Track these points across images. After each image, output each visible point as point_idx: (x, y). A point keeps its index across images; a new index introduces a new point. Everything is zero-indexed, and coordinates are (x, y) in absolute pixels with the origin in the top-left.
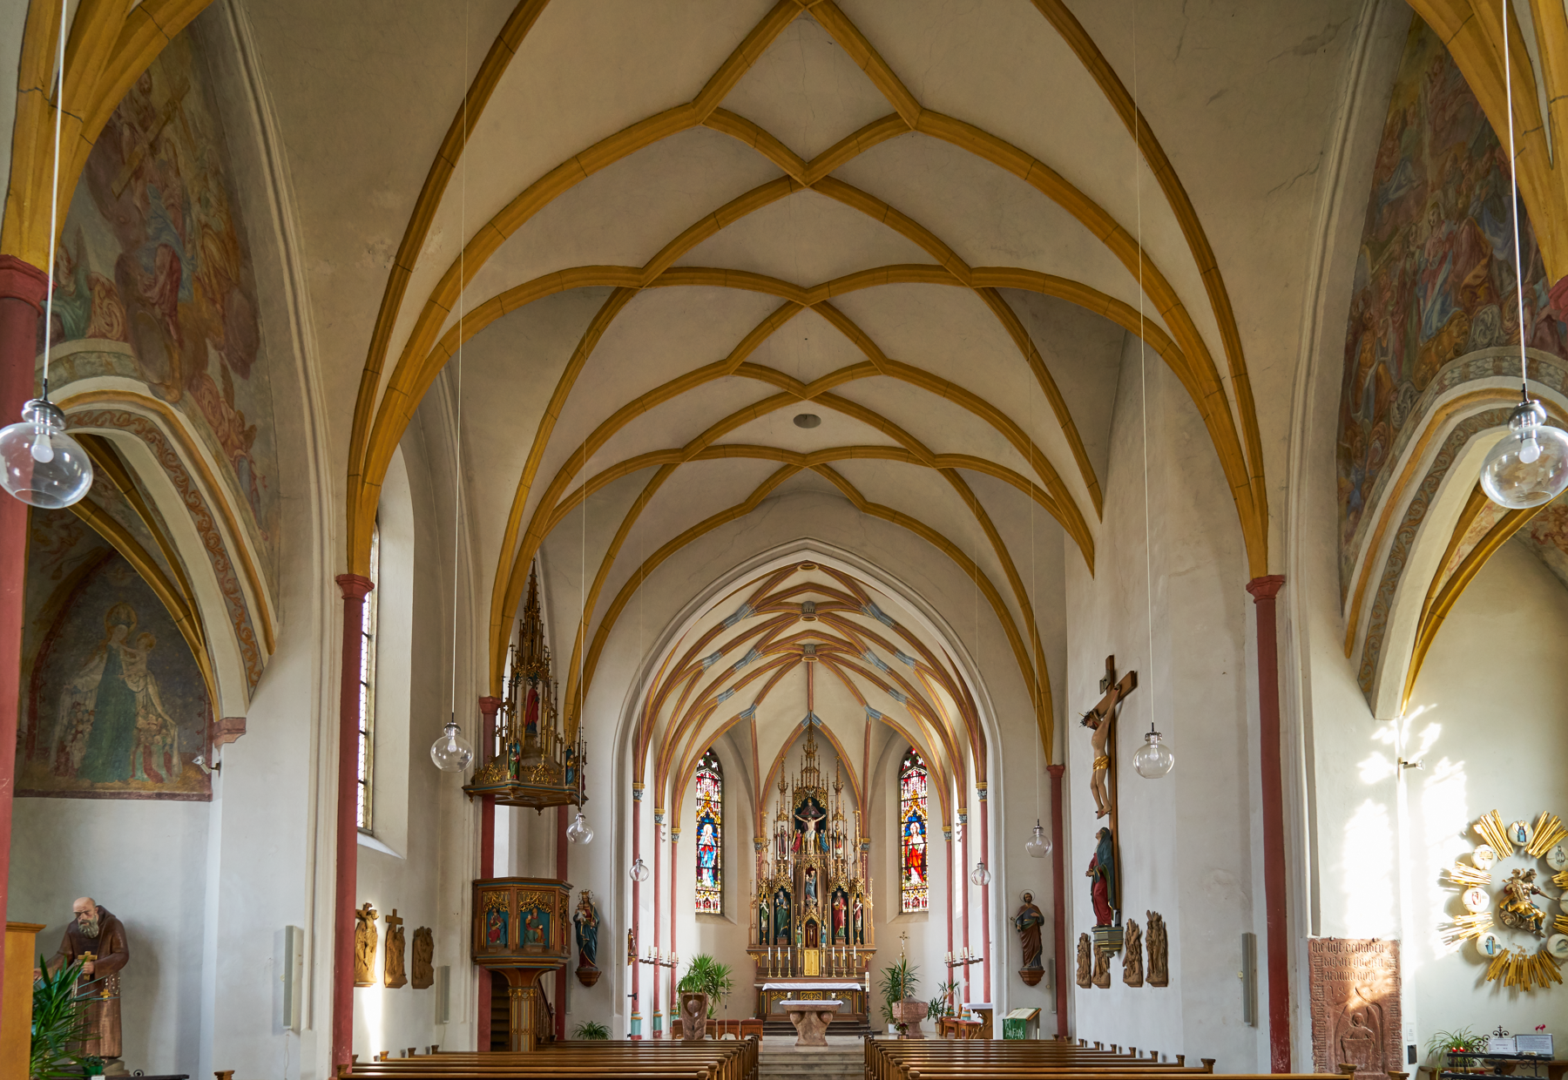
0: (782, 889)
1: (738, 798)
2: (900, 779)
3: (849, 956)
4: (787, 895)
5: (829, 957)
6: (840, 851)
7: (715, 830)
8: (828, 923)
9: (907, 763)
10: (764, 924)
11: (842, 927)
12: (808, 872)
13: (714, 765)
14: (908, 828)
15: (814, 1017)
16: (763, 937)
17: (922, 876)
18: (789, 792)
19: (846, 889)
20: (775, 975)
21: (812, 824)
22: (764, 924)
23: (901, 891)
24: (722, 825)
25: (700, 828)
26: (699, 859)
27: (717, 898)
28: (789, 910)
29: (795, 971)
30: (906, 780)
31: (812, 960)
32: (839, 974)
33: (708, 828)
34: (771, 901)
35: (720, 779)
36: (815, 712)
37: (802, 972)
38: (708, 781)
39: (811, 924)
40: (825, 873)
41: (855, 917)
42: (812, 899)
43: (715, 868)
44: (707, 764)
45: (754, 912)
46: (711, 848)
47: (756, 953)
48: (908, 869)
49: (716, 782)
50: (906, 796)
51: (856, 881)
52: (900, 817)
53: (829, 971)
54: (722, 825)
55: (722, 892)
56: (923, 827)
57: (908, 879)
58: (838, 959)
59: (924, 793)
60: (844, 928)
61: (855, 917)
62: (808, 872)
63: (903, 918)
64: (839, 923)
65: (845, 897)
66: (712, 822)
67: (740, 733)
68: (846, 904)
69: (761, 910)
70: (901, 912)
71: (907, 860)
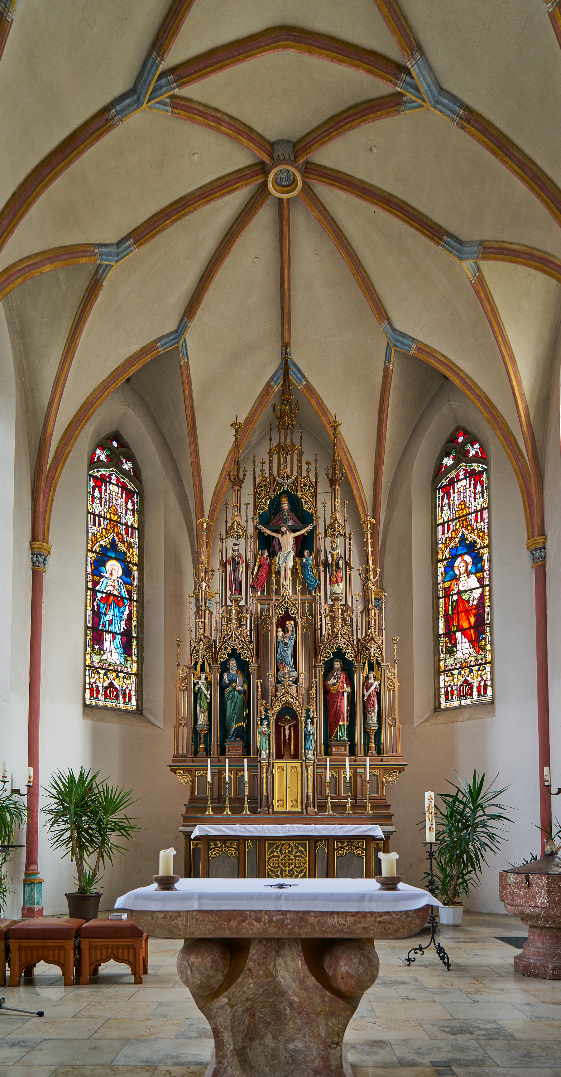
0: (234, 654)
1: (167, 515)
2: (435, 490)
3: (218, 774)
4: (243, 667)
5: (320, 777)
6: (339, 589)
7: (127, 572)
8: (317, 711)
9: (448, 461)
10: (202, 718)
11: (344, 723)
12: (282, 624)
13: (127, 466)
14: (450, 567)
15: (290, 971)
16: (200, 740)
17: (475, 643)
18: (248, 488)
19: (350, 655)
20: (219, 809)
21: (288, 541)
22: (202, 718)
23: (438, 673)
24: (140, 566)
25: (100, 563)
26: (97, 615)
27: (131, 684)
28: (247, 694)
29: (257, 803)
30: (446, 491)
31: (288, 782)
32: (339, 807)
33: (114, 568)
34: (214, 676)
35: (135, 486)
36: (297, 357)
37: (270, 805)
38: (114, 489)
39: (287, 714)
40: (312, 629)
41: (366, 705)
42: (287, 670)
43: (126, 635)
44: (114, 461)
45: (184, 699)
46: (119, 601)
47: (188, 770)
48: (450, 635)
49: (130, 494)
50: (446, 514)
51: (369, 638)
52: (434, 552)
53: (319, 803)
54: (140, 566)
55: (139, 675)
56: (477, 559)
57: (451, 651)
58: (335, 780)
59: (481, 502)
60: (346, 724)
61: (366, 705)
62: (282, 624)
63: (442, 718)
64: (338, 716)
65: (348, 669)
66: (121, 558)
67: (154, 378)
68: (351, 681)
69: (196, 694)
70: (437, 708)
71: (448, 620)
